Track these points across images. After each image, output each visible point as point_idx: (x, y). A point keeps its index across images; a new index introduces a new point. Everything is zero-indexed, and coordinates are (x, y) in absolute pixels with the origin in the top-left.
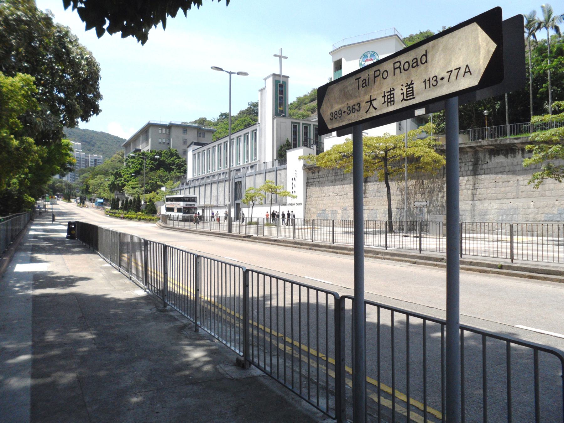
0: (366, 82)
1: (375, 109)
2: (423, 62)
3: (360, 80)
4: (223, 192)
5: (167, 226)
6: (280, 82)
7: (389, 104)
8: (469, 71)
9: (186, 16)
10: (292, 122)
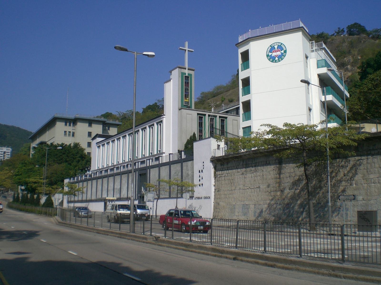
4: (127, 184)
9: (306, 54)
10: (198, 114)
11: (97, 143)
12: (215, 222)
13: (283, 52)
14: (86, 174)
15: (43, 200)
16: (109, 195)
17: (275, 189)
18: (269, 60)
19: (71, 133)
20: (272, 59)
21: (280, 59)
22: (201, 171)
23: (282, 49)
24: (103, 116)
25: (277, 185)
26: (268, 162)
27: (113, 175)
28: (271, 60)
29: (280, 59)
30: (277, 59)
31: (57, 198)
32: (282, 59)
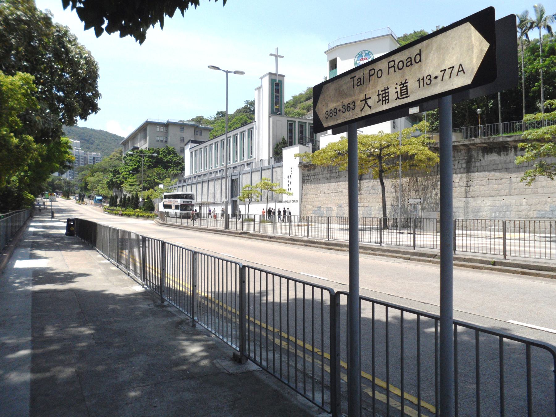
0: (360, 81)
1: (370, 107)
2: (417, 61)
3: (355, 79)
4: (220, 189)
5: (165, 222)
6: (276, 80)
7: (384, 102)
8: (463, 70)
10: (288, 121)
12: (390, 240)
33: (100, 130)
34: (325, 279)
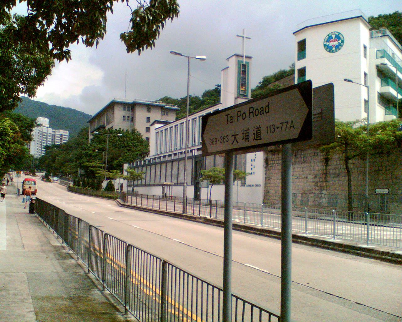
0: (232, 119)
1: (237, 142)
2: (267, 111)
3: (229, 116)
5: (125, 204)
6: (242, 62)
7: (246, 141)
8: (293, 126)
11: (155, 129)
13: (340, 41)
14: (145, 159)
15: (104, 184)
16: (167, 180)
17: (321, 180)
18: (326, 50)
19: (130, 118)
20: (329, 49)
21: (337, 49)
22: (253, 160)
23: (340, 39)
24: (161, 100)
25: (324, 176)
26: (316, 154)
27: (172, 161)
28: (328, 50)
29: (337, 49)
30: (334, 49)
31: (117, 182)
32: (339, 49)
33: (69, 108)
34: (258, 269)
